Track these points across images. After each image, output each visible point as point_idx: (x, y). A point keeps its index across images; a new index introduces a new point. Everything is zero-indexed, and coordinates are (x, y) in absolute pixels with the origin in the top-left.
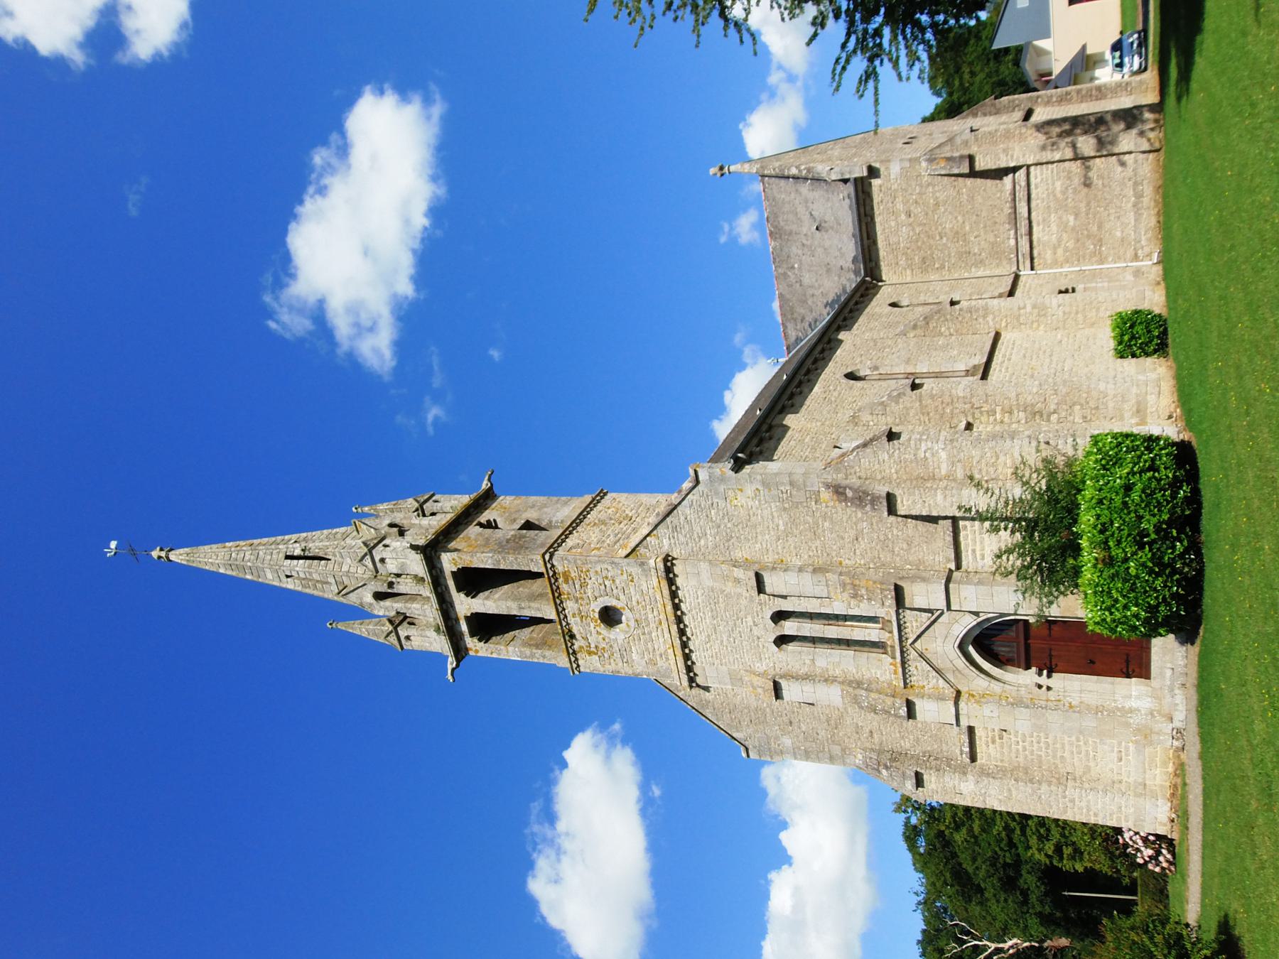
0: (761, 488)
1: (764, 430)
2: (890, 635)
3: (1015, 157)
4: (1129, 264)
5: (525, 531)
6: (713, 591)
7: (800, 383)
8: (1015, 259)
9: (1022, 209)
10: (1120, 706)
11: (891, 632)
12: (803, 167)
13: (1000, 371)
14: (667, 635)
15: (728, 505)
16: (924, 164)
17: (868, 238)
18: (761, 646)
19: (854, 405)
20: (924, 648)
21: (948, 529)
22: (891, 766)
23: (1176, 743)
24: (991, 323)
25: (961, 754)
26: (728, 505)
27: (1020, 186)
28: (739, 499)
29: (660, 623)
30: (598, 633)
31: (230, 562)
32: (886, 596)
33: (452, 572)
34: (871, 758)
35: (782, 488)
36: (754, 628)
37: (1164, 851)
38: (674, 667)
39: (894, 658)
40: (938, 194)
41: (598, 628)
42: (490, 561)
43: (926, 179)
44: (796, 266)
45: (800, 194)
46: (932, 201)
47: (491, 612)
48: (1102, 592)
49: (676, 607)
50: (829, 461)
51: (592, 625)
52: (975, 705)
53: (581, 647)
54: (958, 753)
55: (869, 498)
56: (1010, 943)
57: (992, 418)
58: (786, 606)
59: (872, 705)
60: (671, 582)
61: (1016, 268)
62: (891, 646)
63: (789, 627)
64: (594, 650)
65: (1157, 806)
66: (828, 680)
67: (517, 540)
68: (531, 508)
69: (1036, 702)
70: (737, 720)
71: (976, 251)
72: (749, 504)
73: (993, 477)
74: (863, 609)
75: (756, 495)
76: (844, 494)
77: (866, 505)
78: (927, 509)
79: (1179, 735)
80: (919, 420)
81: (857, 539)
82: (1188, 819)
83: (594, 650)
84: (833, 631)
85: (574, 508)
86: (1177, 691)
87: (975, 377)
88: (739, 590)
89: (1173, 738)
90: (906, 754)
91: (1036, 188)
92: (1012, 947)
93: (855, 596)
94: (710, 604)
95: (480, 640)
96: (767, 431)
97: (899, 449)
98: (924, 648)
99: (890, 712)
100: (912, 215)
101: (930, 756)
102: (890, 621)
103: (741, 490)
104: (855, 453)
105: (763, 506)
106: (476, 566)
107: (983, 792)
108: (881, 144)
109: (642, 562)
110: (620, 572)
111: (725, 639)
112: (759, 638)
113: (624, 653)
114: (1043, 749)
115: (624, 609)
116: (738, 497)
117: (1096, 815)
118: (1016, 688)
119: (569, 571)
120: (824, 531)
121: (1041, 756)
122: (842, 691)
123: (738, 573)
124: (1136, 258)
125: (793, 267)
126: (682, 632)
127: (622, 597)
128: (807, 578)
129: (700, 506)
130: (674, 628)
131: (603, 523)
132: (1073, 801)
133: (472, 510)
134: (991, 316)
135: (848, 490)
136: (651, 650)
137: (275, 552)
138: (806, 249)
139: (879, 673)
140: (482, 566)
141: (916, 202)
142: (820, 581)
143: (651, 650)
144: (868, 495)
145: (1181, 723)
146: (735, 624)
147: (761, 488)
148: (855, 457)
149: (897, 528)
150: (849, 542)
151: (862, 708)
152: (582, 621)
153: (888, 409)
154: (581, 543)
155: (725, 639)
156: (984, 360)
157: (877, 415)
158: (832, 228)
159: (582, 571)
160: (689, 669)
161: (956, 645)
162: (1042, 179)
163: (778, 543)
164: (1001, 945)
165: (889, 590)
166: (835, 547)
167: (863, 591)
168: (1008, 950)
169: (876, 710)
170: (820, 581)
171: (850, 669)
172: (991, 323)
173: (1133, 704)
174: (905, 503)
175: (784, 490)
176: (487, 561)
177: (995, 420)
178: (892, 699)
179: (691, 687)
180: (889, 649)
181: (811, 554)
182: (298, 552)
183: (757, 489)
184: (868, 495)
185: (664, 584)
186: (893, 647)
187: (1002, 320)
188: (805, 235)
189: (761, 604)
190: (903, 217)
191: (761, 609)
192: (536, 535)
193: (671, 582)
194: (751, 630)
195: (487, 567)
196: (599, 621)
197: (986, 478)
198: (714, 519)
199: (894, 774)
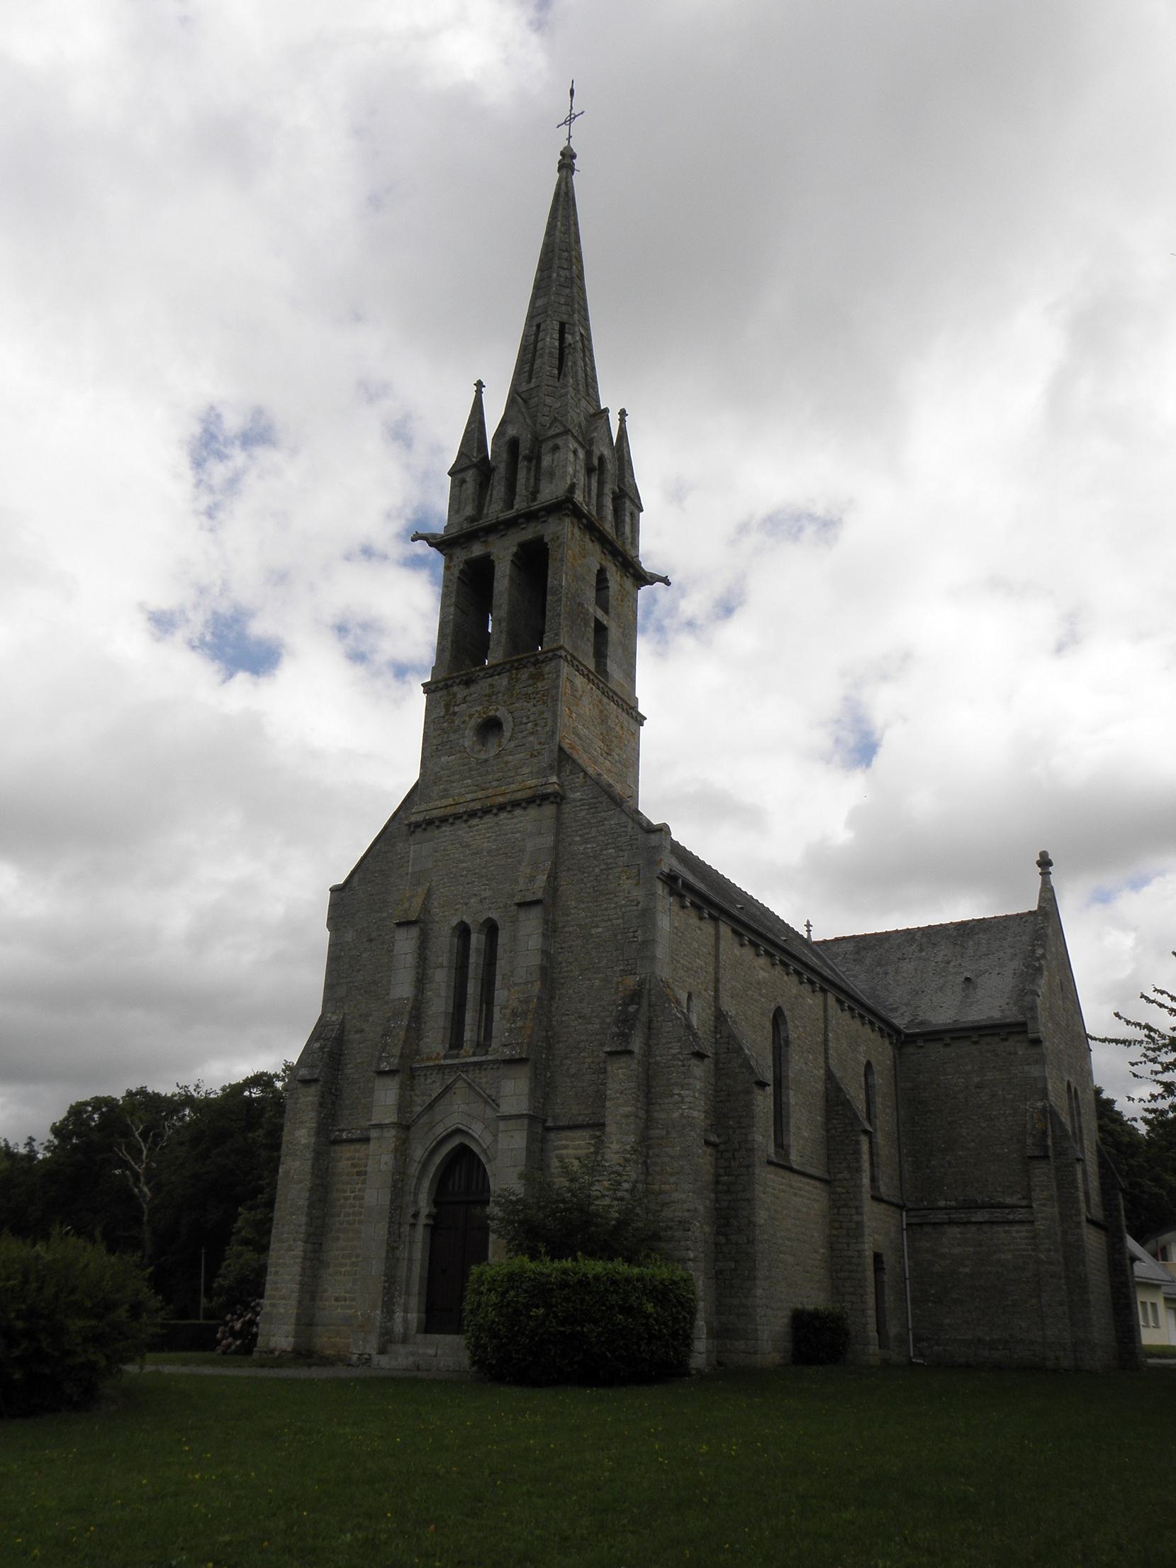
0: (640, 907)
1: (712, 912)
2: (471, 1053)
3: (1042, 1208)
4: (910, 1332)
5: (593, 625)
6: (520, 850)
7: (771, 956)
8: (922, 1207)
9: (980, 1216)
10: (395, 1300)
11: (474, 1055)
12: (1043, 962)
13: (782, 1184)
14: (469, 797)
15: (620, 869)
16: (1039, 1104)
17: (952, 1038)
18: (457, 906)
19: (742, 1017)
20: (456, 1091)
21: (590, 1119)
22: (324, 1052)
23: (355, 1357)
24: (840, 1176)
25: (339, 1130)
26: (620, 869)
27: (1007, 1214)
28: (627, 882)
29: (483, 789)
30: (471, 716)
31: (556, 250)
32: (514, 1049)
33: (543, 536)
34: (332, 1030)
35: (639, 932)
36: (479, 898)
37: (238, 1342)
38: (432, 805)
39: (445, 1057)
40: (1002, 1120)
41: (477, 715)
42: (555, 582)
43: (1022, 1107)
44: (924, 954)
45: (1011, 960)
46: (995, 1113)
47: (495, 584)
48: (513, 1278)
49: (502, 808)
50: (672, 986)
51: (479, 708)
52: (393, 1145)
53: (454, 695)
54: (340, 1127)
55: (626, 1031)
56: (146, 1189)
57: (721, 1171)
58: (503, 938)
59: (391, 1032)
60: (530, 801)
61: (911, 1207)
62: (458, 1054)
63: (476, 940)
64: (451, 711)
65: (287, 1337)
66: (421, 982)
67: (582, 616)
68: (623, 633)
69: (398, 1212)
70: (373, 879)
71: (933, 1162)
72: (621, 894)
73: (650, 1170)
74: (500, 1023)
75: (632, 901)
76: (632, 1002)
77: (619, 1028)
78: (613, 1096)
79: (363, 1360)
80: (722, 1090)
81: (579, 1017)
82: (272, 1367)
83: (451, 711)
84: (472, 988)
85: (622, 685)
86: (411, 1359)
87: (773, 1155)
88: (521, 881)
89: (360, 1355)
90: (339, 1070)
91: (1005, 1232)
92: (141, 1191)
93: (514, 1014)
94: (505, 848)
95: (462, 572)
96: (710, 915)
97: (683, 1066)
98: (456, 1091)
99: (383, 1052)
100: (978, 1090)
101: (336, 1096)
102: (486, 1053)
103: (637, 884)
104: (679, 1015)
105: (618, 910)
106: (550, 566)
107: (298, 1153)
108: (1069, 1056)
109: (554, 767)
110: (542, 740)
111: (465, 865)
112: (466, 904)
113: (448, 747)
114: (347, 1219)
115: (500, 746)
116: (630, 881)
117: (277, 1272)
118: (412, 1190)
119: (544, 679)
120: (589, 979)
121: (339, 1216)
122: (407, 999)
123: (542, 879)
124: (918, 1339)
125: (921, 950)
126: (472, 814)
127: (512, 744)
128: (535, 960)
129: (620, 836)
130: (477, 805)
131: (604, 721)
132: (290, 1249)
133: (620, 560)
134: (848, 1176)
135: (636, 1007)
136: (451, 778)
137: (569, 308)
138: (942, 965)
139: (428, 1040)
140: (550, 572)
141: (994, 1096)
142: (531, 974)
143: (451, 778)
144: (630, 1030)
145: (376, 1363)
146: (482, 877)
147: (640, 907)
148: (675, 1015)
149: (593, 1062)
150: (576, 1009)
151: (388, 1021)
152: (486, 695)
153: (735, 1055)
154: (578, 694)
155: (465, 865)
156: (795, 1167)
157: (728, 1043)
158: (967, 996)
159: (543, 695)
160: (430, 822)
161: (460, 1126)
162: (1015, 1238)
163: (575, 927)
164: (142, 1179)
165: (521, 1052)
166: (571, 991)
167: (519, 1024)
168: (138, 1187)
169: (386, 1036)
170: (531, 974)
171: (432, 1008)
172: (840, 1176)
173: (397, 1314)
174: (620, 1071)
175: (636, 934)
176: (556, 580)
177: (720, 1175)
178: (398, 1054)
179: (409, 825)
180: (455, 1052)
181: (564, 964)
182: (569, 338)
183: (639, 903)
184: (630, 1030)
185: (529, 793)
186: (457, 1056)
187: (843, 1187)
188: (960, 965)
189: (505, 907)
190: (977, 1080)
191: (500, 908)
192: (588, 640)
193: (530, 801)
194: (475, 895)
195: (549, 580)
196: (485, 716)
197: (648, 1161)
198: (605, 852)
199: (315, 1056)
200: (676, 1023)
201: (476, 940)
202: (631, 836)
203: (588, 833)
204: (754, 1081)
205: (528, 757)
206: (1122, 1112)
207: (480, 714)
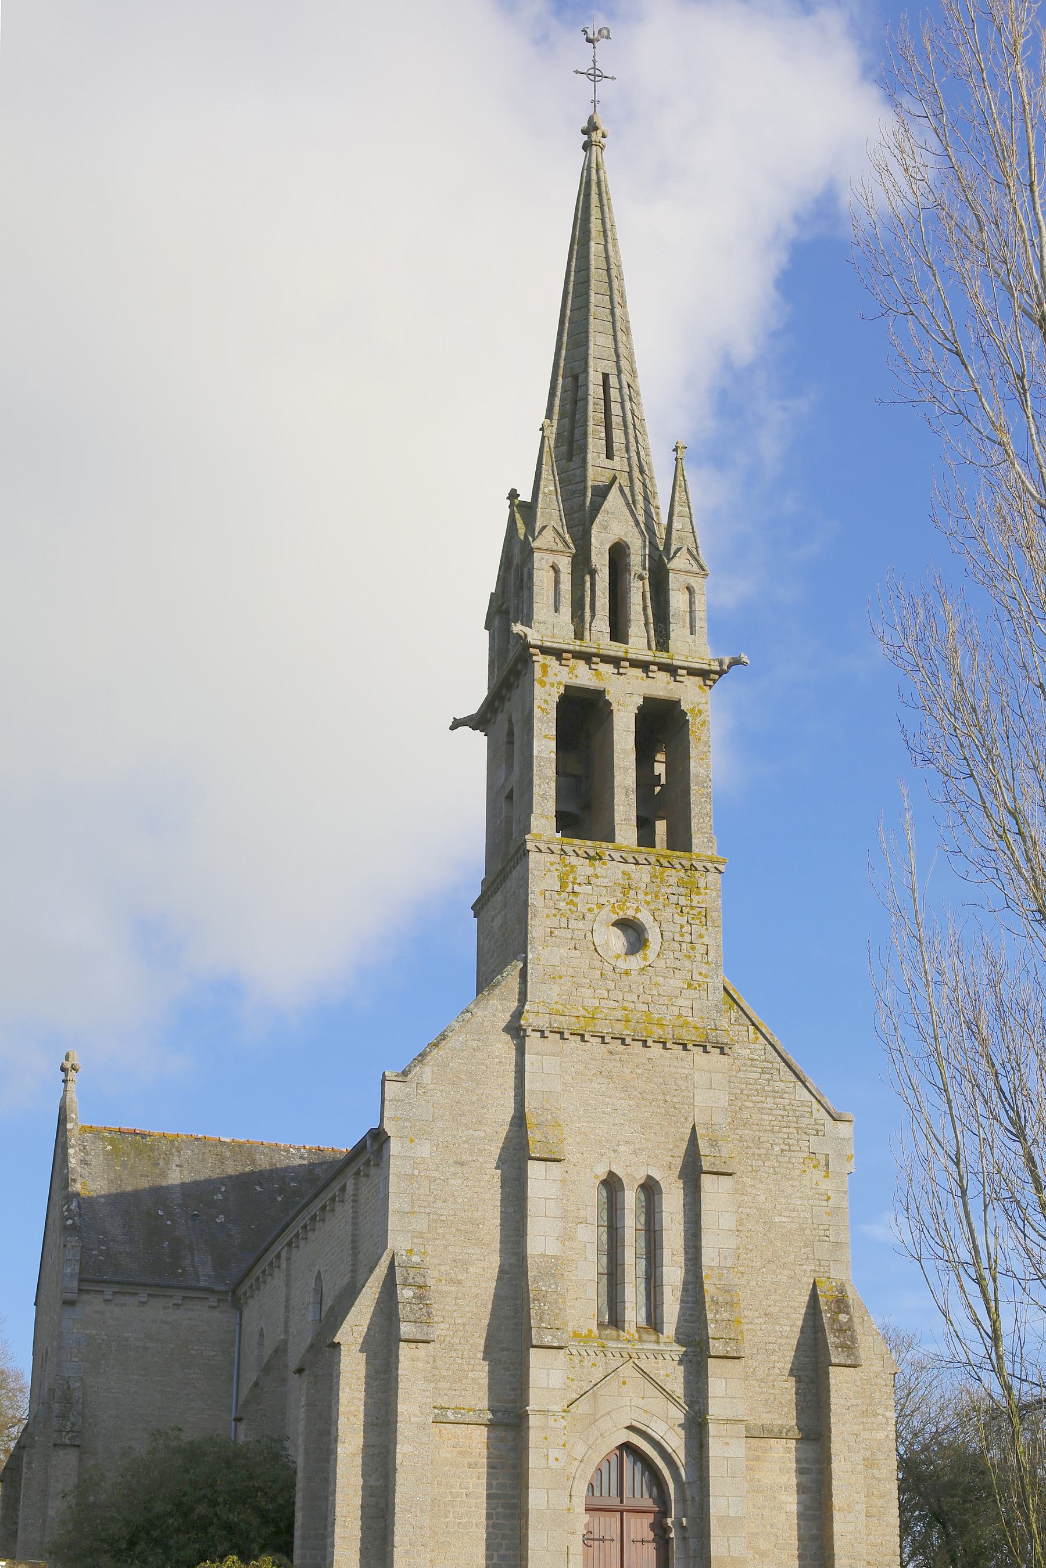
63: (631, 1199)
112: (615, 1151)
200: (877, 1338)
201: (631, 1199)
202: (815, 1120)
203: (761, 1102)
204: (389, 1128)
205: (686, 987)
206: (678, 703)
207: (613, 907)
